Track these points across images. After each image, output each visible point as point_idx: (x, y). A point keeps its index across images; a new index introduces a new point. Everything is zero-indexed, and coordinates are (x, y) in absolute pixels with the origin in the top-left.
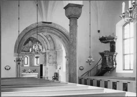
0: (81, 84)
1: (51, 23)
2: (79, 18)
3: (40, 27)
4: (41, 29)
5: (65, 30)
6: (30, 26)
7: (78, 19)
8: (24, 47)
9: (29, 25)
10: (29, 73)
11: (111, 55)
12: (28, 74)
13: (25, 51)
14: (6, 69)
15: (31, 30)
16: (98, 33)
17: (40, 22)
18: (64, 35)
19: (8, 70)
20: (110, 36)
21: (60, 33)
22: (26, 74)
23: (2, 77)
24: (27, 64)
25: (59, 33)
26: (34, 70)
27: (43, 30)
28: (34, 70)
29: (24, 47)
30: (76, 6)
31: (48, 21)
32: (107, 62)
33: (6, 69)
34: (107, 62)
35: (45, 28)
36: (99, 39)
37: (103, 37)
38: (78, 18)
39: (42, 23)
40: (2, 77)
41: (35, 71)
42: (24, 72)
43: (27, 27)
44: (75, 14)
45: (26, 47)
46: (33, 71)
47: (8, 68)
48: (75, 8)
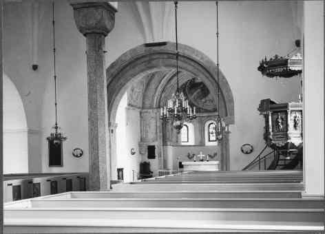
0: (85, 190)
1: (164, 44)
2: (109, 34)
3: (143, 57)
4: (149, 62)
5: (202, 54)
6: (119, 58)
7: (106, 38)
8: (205, 102)
9: (117, 58)
10: (202, 160)
11: (279, 112)
12: (197, 163)
13: (207, 111)
14: (74, 155)
15: (124, 67)
16: (33, 71)
17: (141, 46)
18: (202, 66)
19: (247, 153)
20: (276, 56)
21: (193, 63)
22: (192, 163)
23: (4, 173)
24: (209, 141)
25: (190, 64)
26: (212, 155)
27: (154, 62)
28: (212, 155)
29: (205, 102)
30: (87, 5)
31: (156, 41)
32: (271, 130)
33: (242, 151)
34: (271, 130)
35: (154, 57)
36: (261, 68)
37: (276, 56)
38: (105, 36)
39: (144, 48)
40: (4, 173)
41: (215, 158)
42: (190, 158)
43: (112, 62)
44: (86, 25)
45: (210, 100)
46: (210, 156)
47: (79, 152)
48: (85, 10)
